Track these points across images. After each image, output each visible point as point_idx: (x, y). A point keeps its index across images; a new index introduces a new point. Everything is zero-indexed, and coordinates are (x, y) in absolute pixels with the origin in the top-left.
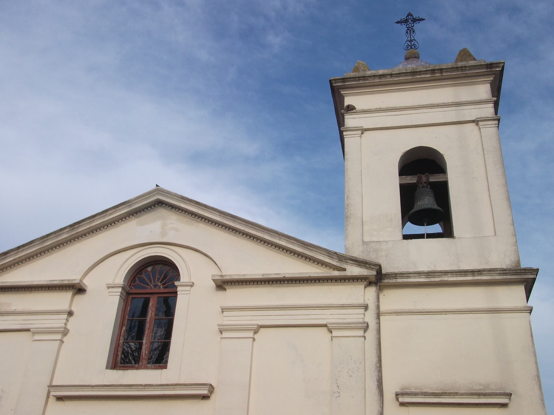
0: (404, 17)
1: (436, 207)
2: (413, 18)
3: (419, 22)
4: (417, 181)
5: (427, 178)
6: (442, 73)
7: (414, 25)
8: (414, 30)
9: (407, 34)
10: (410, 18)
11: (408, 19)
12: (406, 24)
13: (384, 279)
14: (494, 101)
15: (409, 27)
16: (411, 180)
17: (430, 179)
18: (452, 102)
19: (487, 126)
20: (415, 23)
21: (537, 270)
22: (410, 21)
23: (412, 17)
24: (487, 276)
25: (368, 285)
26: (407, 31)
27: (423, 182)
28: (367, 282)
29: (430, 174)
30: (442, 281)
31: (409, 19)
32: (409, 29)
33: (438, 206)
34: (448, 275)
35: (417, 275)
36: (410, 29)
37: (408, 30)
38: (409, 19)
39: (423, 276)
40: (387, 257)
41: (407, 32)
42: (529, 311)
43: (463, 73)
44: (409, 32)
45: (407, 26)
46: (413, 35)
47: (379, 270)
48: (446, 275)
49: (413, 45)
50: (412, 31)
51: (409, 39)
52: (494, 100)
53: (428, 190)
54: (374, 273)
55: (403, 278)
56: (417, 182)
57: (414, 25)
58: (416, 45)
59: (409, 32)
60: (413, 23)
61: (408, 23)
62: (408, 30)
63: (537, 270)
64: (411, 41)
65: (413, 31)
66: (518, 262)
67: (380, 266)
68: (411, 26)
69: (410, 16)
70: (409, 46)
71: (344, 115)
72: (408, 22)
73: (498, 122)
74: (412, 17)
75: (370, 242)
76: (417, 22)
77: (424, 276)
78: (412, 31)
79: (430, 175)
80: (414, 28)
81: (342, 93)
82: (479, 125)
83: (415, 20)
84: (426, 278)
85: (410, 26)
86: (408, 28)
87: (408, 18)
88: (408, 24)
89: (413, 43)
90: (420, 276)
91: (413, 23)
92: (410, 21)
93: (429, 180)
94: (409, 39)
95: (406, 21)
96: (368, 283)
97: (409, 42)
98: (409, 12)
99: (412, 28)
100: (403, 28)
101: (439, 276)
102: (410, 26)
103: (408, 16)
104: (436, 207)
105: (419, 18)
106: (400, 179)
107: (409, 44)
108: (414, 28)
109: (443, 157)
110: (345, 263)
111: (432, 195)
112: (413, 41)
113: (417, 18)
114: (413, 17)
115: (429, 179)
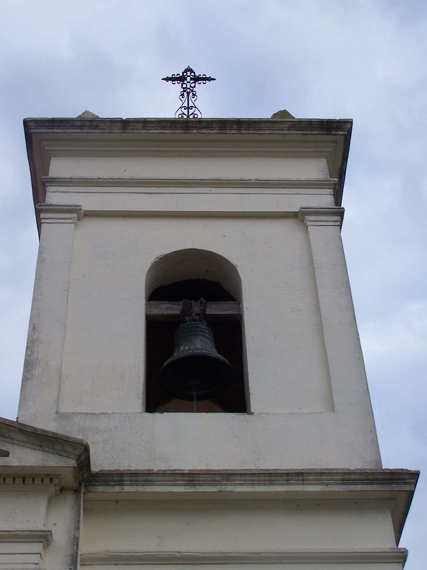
0: (179, 71)
1: (214, 353)
2: (195, 76)
3: (204, 82)
4: (182, 311)
5: (202, 308)
6: (240, 130)
7: (195, 86)
8: (194, 93)
9: (183, 97)
10: (188, 84)
11: (186, 77)
12: (181, 82)
13: (95, 485)
14: (335, 185)
15: (186, 87)
16: (169, 309)
17: (207, 310)
18: (256, 180)
19: (319, 223)
20: (197, 83)
21: (415, 475)
22: (188, 79)
23: (193, 73)
24: (316, 484)
25: (57, 495)
26: (182, 93)
27: (194, 314)
28: (56, 485)
29: (207, 301)
30: (221, 491)
31: (189, 82)
32: (186, 90)
33: (219, 349)
34: (234, 480)
35: (169, 478)
36: (188, 90)
37: (184, 91)
38: (189, 82)
39: (180, 480)
40: (107, 444)
41: (182, 95)
42: (401, 560)
43: (279, 133)
44: (185, 94)
45: (182, 86)
46: (193, 100)
47: (83, 457)
48: (231, 481)
49: (192, 114)
50: (191, 94)
51: (186, 105)
52: (333, 182)
53: (204, 326)
54: (73, 463)
55: (137, 485)
56: (181, 313)
57: (195, 86)
58: (197, 115)
59: (185, 94)
60: (195, 83)
61: (185, 82)
62: (184, 91)
63: (415, 475)
64: (188, 108)
65: (193, 93)
66: (379, 462)
67: (86, 449)
68: (191, 86)
69: (189, 73)
70: (186, 115)
71: (46, 185)
72: (186, 80)
73: (340, 218)
74: (193, 74)
75: (73, 413)
76: (202, 82)
77: (184, 480)
78: (191, 94)
79: (209, 302)
80: (195, 89)
81: (46, 148)
82: (305, 220)
83: (196, 79)
84: (188, 485)
85: (188, 87)
86: (184, 88)
87: (185, 74)
88: (185, 84)
89: (191, 112)
90: (175, 481)
91: (195, 83)
92: (188, 79)
93: (205, 311)
94: (186, 105)
95: (181, 79)
96: (58, 488)
97: (185, 109)
98: (189, 67)
99: (192, 89)
100: (177, 87)
101: (214, 483)
102: (188, 87)
103: (186, 71)
104: (214, 353)
105: (204, 76)
106: (148, 307)
107: (186, 112)
108: (195, 89)
109: (236, 271)
110: (8, 440)
111: (210, 336)
112: (192, 109)
113: (202, 76)
114: (194, 74)
115: (205, 308)
